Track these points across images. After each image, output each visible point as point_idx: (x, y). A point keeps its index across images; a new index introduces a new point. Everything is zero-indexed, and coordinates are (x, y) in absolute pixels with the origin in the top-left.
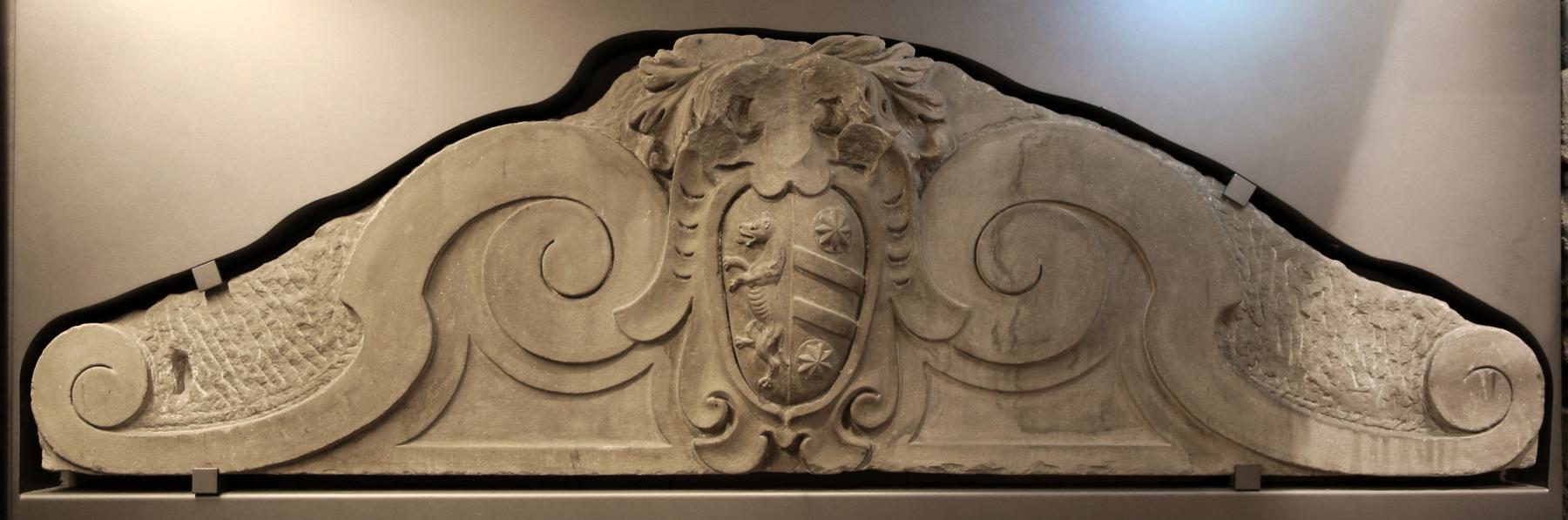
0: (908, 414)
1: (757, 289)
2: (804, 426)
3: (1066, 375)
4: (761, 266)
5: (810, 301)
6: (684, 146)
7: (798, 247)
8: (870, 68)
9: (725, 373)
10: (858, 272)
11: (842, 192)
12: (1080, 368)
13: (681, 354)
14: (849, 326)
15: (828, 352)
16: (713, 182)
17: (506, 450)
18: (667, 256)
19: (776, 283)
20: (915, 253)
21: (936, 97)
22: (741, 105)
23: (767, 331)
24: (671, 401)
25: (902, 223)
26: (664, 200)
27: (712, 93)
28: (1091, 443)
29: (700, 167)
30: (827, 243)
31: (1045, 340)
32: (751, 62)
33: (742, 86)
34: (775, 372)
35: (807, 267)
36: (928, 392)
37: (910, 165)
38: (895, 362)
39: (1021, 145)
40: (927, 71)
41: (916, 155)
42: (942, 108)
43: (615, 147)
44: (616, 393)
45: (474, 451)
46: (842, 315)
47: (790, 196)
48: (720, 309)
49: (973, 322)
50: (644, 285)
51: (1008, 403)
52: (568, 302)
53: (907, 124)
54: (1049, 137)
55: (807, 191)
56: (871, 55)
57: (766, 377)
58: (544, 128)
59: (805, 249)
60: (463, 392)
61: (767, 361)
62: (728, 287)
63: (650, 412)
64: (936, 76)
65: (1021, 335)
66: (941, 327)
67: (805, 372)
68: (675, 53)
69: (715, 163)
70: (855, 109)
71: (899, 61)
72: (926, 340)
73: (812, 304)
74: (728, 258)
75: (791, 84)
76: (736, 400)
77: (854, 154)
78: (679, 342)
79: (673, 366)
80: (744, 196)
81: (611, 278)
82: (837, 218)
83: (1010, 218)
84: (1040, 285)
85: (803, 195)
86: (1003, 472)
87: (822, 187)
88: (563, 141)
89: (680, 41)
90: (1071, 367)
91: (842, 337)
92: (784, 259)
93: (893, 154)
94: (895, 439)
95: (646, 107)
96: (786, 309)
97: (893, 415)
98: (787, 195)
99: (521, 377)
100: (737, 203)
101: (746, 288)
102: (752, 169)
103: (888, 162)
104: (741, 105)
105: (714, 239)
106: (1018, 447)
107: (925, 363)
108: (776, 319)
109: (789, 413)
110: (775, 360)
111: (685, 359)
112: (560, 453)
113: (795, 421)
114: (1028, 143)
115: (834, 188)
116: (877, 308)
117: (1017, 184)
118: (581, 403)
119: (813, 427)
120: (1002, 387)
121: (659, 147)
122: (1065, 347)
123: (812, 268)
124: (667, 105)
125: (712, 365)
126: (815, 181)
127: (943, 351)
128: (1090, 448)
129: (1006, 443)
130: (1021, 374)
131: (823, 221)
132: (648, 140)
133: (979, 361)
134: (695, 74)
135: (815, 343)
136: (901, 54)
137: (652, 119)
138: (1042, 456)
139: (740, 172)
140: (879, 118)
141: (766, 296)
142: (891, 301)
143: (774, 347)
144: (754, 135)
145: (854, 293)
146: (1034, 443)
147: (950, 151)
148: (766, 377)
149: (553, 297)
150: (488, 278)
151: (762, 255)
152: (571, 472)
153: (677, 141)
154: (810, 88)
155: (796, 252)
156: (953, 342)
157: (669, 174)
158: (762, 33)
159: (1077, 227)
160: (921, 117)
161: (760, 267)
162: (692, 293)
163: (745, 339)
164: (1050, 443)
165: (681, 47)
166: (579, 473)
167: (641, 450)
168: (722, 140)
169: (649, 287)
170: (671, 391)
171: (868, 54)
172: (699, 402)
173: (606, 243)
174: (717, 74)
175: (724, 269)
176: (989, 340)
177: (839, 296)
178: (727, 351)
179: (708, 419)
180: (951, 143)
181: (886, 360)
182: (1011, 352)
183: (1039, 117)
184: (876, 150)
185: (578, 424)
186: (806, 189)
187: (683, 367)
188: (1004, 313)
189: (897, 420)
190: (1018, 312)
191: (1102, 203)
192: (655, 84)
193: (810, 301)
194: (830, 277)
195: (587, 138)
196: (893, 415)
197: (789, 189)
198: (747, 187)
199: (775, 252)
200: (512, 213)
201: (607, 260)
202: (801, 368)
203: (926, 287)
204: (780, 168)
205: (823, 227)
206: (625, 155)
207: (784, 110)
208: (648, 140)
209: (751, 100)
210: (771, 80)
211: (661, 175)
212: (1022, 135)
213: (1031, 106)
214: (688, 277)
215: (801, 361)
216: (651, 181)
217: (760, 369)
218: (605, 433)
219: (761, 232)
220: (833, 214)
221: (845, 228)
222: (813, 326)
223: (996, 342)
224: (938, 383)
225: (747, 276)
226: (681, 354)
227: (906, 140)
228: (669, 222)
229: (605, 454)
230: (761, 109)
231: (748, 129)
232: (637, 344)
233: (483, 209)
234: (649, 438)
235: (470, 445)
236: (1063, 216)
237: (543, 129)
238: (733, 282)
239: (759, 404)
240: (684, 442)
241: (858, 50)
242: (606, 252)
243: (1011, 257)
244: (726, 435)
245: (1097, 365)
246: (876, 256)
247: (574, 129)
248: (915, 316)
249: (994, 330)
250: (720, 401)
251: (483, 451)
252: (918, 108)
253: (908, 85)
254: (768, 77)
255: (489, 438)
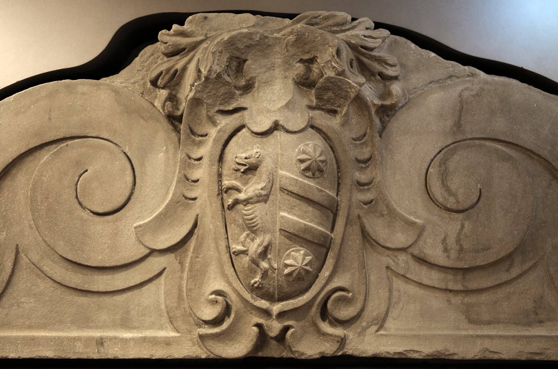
0: (375, 307)
1: (250, 207)
2: (288, 319)
3: (505, 277)
4: (254, 187)
5: (294, 217)
6: (191, 95)
7: (281, 172)
8: (339, 35)
9: (224, 275)
10: (334, 195)
11: (319, 130)
12: (515, 272)
13: (188, 260)
14: (326, 237)
15: (308, 258)
16: (214, 124)
17: (43, 338)
18: (178, 182)
19: (266, 201)
20: (378, 179)
21: (391, 59)
22: (238, 64)
23: (258, 241)
24: (180, 298)
25: (367, 156)
26: (176, 139)
27: (214, 53)
28: (527, 333)
29: (204, 112)
30: (307, 169)
31: (487, 249)
32: (245, 31)
33: (238, 49)
34: (265, 274)
35: (291, 188)
36: (390, 291)
37: (373, 110)
38: (363, 266)
39: (460, 95)
40: (384, 39)
41: (377, 102)
42: (398, 68)
43: (138, 97)
44: (136, 292)
45: (17, 338)
46: (320, 228)
47: (276, 133)
48: (220, 224)
49: (426, 234)
50: (159, 206)
51: (457, 300)
52: (97, 219)
53: (368, 80)
54: (482, 89)
55: (290, 128)
56: (341, 26)
57: (257, 279)
58: (83, 84)
59: (288, 174)
60: (10, 290)
61: (258, 265)
62: (226, 206)
63: (163, 307)
64: (390, 45)
65: (466, 245)
66: (400, 239)
67: (290, 274)
68: (187, 27)
69: (217, 108)
70: (328, 65)
71: (361, 32)
72: (388, 248)
73: (295, 218)
74: (226, 183)
75: (277, 48)
76: (233, 298)
77: (328, 101)
78: (186, 251)
79: (182, 271)
80: (239, 134)
81: (132, 200)
82: (315, 150)
83: (454, 152)
84: (480, 204)
85: (288, 131)
86: (456, 357)
87: (303, 126)
88: (98, 95)
89: (190, 17)
90: (508, 270)
91: (320, 246)
92: (272, 182)
93: (359, 100)
94: (365, 329)
95: (163, 68)
96: (274, 222)
97: (362, 310)
98: (275, 134)
99: (58, 279)
100: (234, 139)
101: (240, 206)
102: (246, 113)
103: (351, 102)
104: (238, 64)
105: (215, 168)
106: (467, 337)
107: (388, 268)
108: (265, 231)
109: (276, 308)
110: (264, 265)
111: (191, 264)
112: (88, 340)
113: (282, 315)
114: (466, 94)
115: (312, 127)
116: (348, 222)
117: (458, 125)
118: (107, 299)
119: (297, 320)
120: (451, 286)
121: (172, 98)
122: (503, 254)
123: (295, 190)
124: (179, 66)
125: (213, 269)
126: (297, 121)
127: (402, 257)
128: (527, 337)
129: (457, 333)
130: (466, 276)
131: (304, 152)
132: (164, 93)
133: (431, 265)
134: (201, 42)
135: (298, 251)
136: (363, 26)
137: (167, 77)
138: (487, 344)
139: (237, 115)
140: (348, 73)
141: (257, 212)
142: (359, 217)
143: (264, 254)
144: (248, 88)
145: (329, 210)
146: (480, 333)
147: (403, 101)
148: (257, 279)
149: (85, 215)
150: (33, 200)
151: (254, 179)
152: (96, 356)
153: (186, 92)
154: (292, 50)
155: (282, 177)
156: (410, 250)
157: (180, 119)
158: (254, 13)
159: (507, 158)
160: (381, 74)
161: (252, 189)
162: (198, 211)
163: (240, 248)
164: (493, 333)
165: (191, 22)
166: (103, 356)
167: (154, 338)
168: (222, 90)
169: (163, 206)
170: (180, 290)
171: (338, 25)
172: (203, 300)
173: (129, 171)
174: (219, 39)
175: (223, 191)
176: (440, 248)
177: (317, 213)
178: (225, 257)
179: (210, 313)
180: (404, 95)
181: (356, 265)
182: (459, 259)
183: (473, 75)
184: (346, 98)
185: (104, 317)
186: (290, 127)
187: (190, 270)
188: (452, 227)
189: (366, 314)
190: (463, 226)
191: (527, 139)
192: (170, 50)
193: (294, 217)
194: (310, 197)
195: (116, 92)
196: (362, 310)
197: (276, 127)
198: (242, 127)
199: (264, 177)
200: (54, 149)
201: (130, 185)
202: (287, 271)
203: (388, 206)
204: (269, 111)
205: (303, 157)
206: (146, 105)
207: (271, 68)
208: (164, 93)
209: (245, 61)
210: (261, 46)
211: (174, 120)
212: (460, 88)
213: (466, 68)
214: (195, 199)
215: (287, 266)
216: (165, 124)
217: (253, 272)
218: (125, 324)
219: (253, 160)
220: (312, 147)
221: (322, 158)
222: (296, 237)
223: (446, 250)
224: (398, 283)
225: (242, 196)
226: (188, 260)
227: (370, 93)
228: (180, 155)
229: (125, 341)
230: (253, 67)
231: (243, 83)
232: (152, 252)
233: (32, 146)
234: (161, 328)
235: (15, 333)
236: (497, 150)
237: (83, 85)
238: (230, 201)
239: (251, 301)
240: (190, 332)
241: (331, 22)
242: (129, 179)
243: (455, 183)
244: (225, 326)
245: (529, 269)
246: (347, 182)
247: (108, 85)
248: (378, 228)
249: (444, 241)
250: (220, 298)
251: (24, 338)
252: (377, 67)
253: (372, 49)
254: (258, 44)
255: (30, 327)
